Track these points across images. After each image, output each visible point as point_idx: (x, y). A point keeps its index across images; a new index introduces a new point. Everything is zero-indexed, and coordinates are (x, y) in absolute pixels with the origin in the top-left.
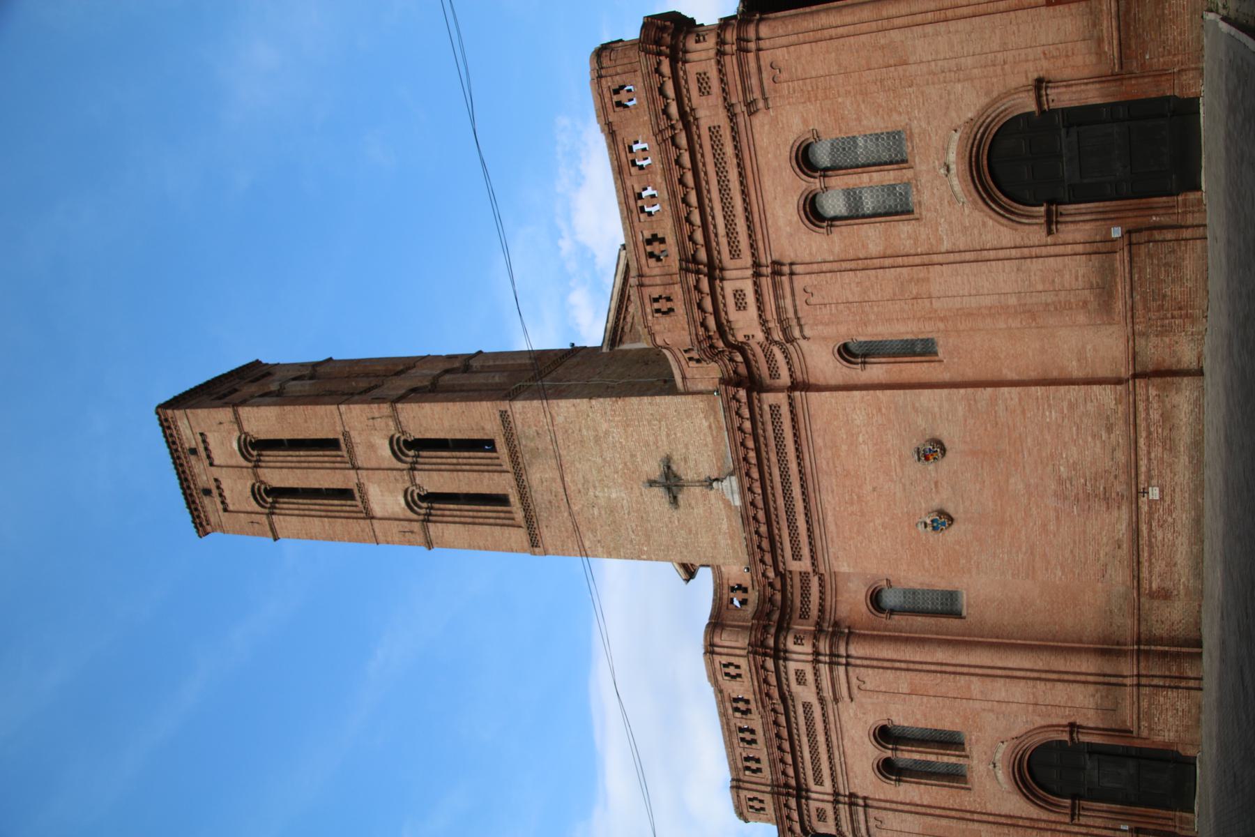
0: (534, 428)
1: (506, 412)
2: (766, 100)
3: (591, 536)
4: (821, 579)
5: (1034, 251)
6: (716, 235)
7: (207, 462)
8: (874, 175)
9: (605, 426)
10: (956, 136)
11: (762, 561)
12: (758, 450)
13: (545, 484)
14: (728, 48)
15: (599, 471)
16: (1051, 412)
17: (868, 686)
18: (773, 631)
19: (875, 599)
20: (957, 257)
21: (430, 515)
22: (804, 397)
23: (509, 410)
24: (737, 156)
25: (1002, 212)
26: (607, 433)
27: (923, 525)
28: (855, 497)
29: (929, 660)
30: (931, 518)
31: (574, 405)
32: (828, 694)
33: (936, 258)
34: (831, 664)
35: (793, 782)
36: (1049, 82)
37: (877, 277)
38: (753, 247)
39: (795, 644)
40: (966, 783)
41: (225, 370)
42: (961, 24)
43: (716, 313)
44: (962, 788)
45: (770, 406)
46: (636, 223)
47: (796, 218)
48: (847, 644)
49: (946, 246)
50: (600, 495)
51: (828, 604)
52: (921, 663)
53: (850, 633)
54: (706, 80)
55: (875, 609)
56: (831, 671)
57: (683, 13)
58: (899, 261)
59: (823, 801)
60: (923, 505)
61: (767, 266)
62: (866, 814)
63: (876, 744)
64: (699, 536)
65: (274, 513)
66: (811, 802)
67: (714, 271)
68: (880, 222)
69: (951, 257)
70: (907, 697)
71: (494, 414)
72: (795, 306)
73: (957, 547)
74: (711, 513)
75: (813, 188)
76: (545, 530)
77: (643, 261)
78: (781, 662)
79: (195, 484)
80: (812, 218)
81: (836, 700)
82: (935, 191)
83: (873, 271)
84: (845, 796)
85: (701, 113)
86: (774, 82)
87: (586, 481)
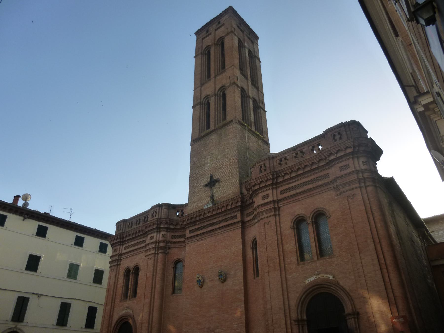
0: (228, 133)
1: (233, 122)
2: (340, 194)
3: (196, 160)
4: (183, 242)
5: (288, 315)
6: (288, 184)
7: (216, 28)
8: (314, 244)
9: (229, 157)
10: (331, 277)
11: (188, 219)
12: (221, 212)
13: (211, 140)
14: (360, 175)
15: (215, 158)
16: (236, 324)
17: (149, 262)
18: (166, 226)
19: (177, 262)
20: (284, 282)
21: (203, 105)
22: (240, 227)
23: (233, 123)
24: (318, 186)
25: (302, 300)
26: (227, 158)
27: (198, 276)
28: (208, 250)
29: (156, 283)
30: (201, 279)
31: (235, 145)
32: (148, 247)
33: (283, 272)
34: (155, 248)
35: (124, 240)
36: (358, 318)
37: (275, 249)
38: (285, 199)
39: (162, 234)
40: (123, 300)
41: (252, 27)
42: (379, 276)
43: (260, 188)
44: (121, 298)
45: (236, 215)
46: (291, 152)
47: (296, 214)
48: (162, 253)
49: (289, 277)
50: (208, 160)
51: (177, 245)
52: (155, 280)
53: (166, 254)
54: (347, 168)
55: (175, 262)
56: (153, 248)
57: (382, 155)
58: (282, 258)
59: (119, 250)
60: (206, 276)
61: (278, 205)
62: (115, 265)
63: (134, 266)
64: (196, 196)
65: (202, 54)
66: (119, 246)
67: (275, 185)
68: (296, 248)
69: (284, 279)
70: (145, 276)
71: (232, 118)
72: (264, 218)
73: (193, 290)
74: (203, 199)
75: (308, 219)
76: (198, 144)
77: (279, 158)
78: (156, 230)
79: (210, 26)
80: (297, 220)
81: (145, 251)
82: (309, 270)
83: (277, 248)
84: (121, 258)
85: (333, 169)
86: (347, 197)
87: (212, 154)
